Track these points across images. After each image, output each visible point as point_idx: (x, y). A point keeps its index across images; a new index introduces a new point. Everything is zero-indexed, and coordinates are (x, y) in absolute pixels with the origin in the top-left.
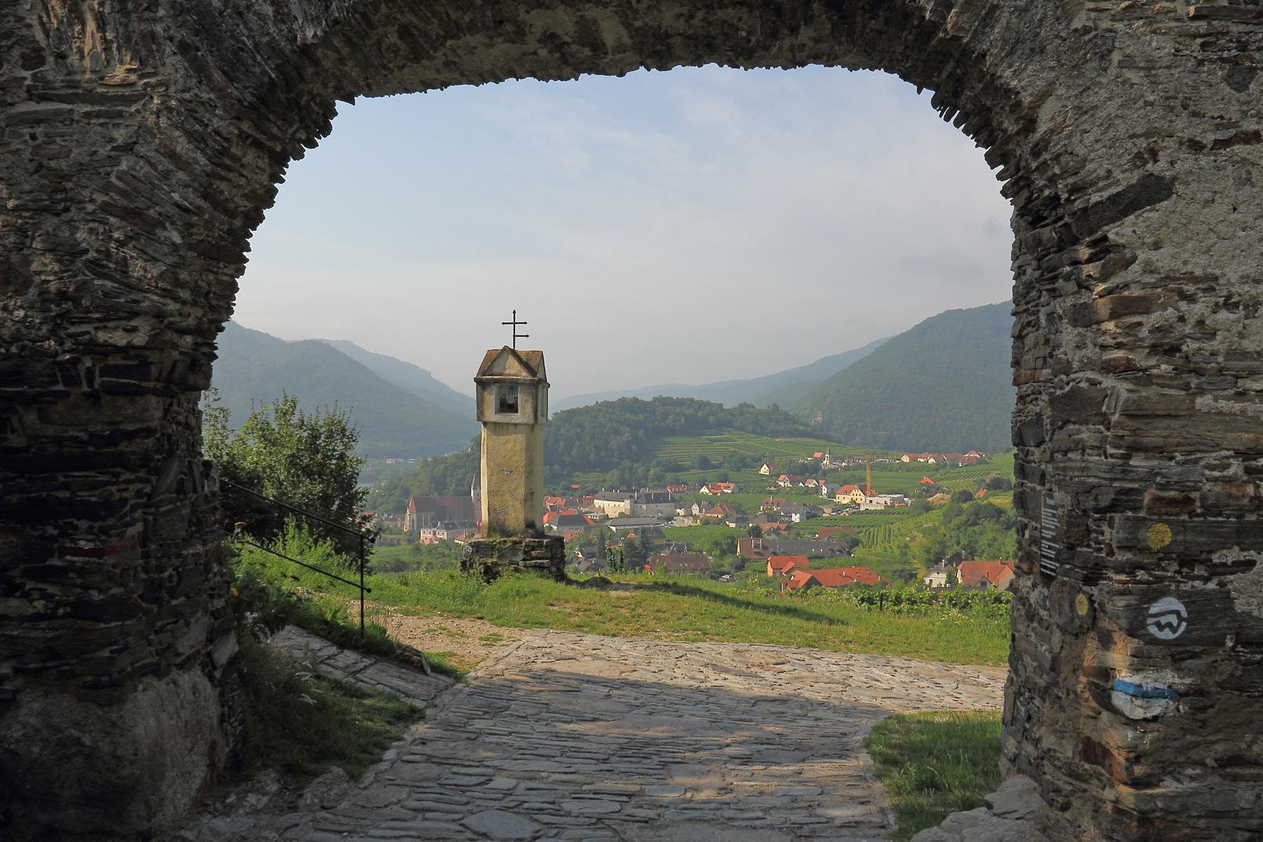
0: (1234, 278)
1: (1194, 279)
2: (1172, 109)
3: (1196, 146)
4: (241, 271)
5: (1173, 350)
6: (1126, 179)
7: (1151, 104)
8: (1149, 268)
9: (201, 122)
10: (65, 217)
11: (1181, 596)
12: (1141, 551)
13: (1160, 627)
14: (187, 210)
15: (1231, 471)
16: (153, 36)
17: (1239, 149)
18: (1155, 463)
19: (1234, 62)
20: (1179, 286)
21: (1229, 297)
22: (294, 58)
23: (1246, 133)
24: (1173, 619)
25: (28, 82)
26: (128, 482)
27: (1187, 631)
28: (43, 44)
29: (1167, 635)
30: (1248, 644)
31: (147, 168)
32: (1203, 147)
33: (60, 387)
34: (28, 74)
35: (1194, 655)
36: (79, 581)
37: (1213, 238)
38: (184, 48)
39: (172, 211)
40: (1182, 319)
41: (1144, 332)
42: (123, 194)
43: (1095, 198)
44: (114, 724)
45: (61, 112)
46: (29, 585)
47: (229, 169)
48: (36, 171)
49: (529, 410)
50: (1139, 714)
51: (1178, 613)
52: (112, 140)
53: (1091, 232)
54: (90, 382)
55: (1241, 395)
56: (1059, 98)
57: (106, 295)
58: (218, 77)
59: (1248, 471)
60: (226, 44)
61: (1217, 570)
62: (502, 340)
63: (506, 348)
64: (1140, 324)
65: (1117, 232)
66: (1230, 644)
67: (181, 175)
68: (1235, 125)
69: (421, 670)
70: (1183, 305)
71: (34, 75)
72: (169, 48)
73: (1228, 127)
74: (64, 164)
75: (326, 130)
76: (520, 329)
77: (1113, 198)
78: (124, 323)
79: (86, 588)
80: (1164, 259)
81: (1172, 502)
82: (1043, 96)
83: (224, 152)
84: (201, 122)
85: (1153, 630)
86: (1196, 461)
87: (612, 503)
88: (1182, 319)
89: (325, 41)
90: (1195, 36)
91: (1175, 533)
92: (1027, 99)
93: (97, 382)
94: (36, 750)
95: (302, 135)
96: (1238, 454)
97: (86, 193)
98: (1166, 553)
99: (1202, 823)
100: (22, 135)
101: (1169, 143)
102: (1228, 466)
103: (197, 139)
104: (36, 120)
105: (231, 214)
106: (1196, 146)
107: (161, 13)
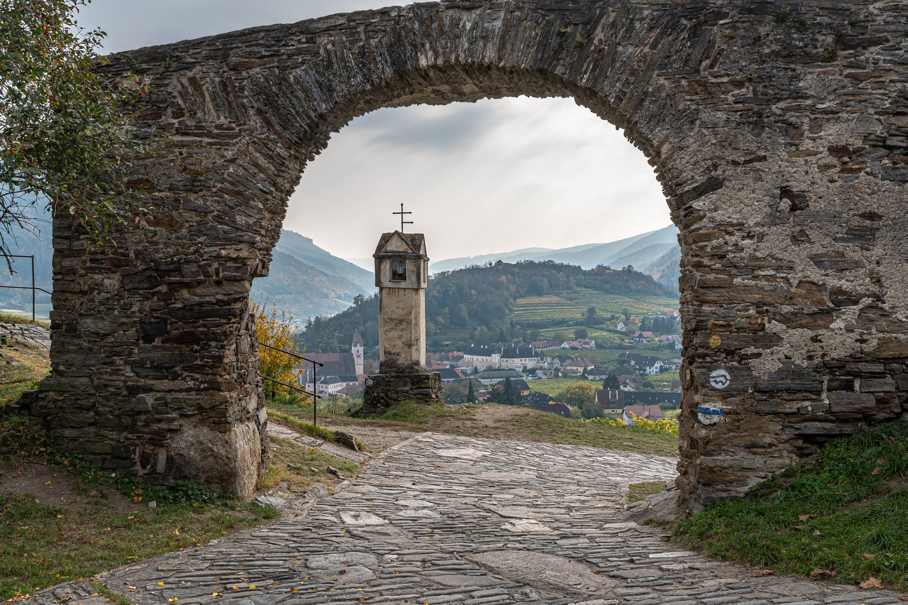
0: (751, 223)
1: (732, 225)
2: (724, 146)
3: (735, 163)
4: (283, 217)
5: (722, 257)
6: (701, 179)
7: (714, 144)
8: (712, 220)
9: (271, 150)
10: (201, 194)
11: (726, 369)
12: (707, 348)
13: (715, 381)
14: (266, 192)
15: (751, 312)
16: (243, 106)
17: (757, 165)
18: (713, 308)
19: (756, 123)
20: (725, 228)
21: (749, 233)
22: (316, 120)
23: (759, 157)
24: (723, 379)
25: (176, 126)
26: (233, 323)
27: (730, 385)
28: (183, 106)
29: (719, 386)
30: (759, 391)
31: (243, 171)
32: (739, 164)
33: (202, 277)
34: (176, 121)
35: (733, 396)
36: (210, 371)
37: (743, 205)
38: (259, 112)
39: (256, 191)
40: (726, 243)
41: (709, 249)
42: (232, 184)
43: (686, 189)
44: (227, 442)
45: (196, 142)
46: (185, 374)
47: (284, 172)
48: (184, 171)
49: (414, 278)
50: (707, 422)
51: (725, 376)
52: (223, 156)
53: (685, 204)
54: (217, 274)
55: (755, 277)
56: (670, 143)
57: (225, 232)
58: (278, 128)
59: (758, 312)
60: (281, 111)
61: (743, 358)
62: (393, 225)
63: (396, 232)
64: (707, 246)
65: (697, 204)
66: (750, 391)
67: (261, 175)
68: (754, 153)
69: (352, 448)
70: (727, 237)
71: (180, 122)
72: (251, 112)
73: (750, 154)
74: (198, 168)
75: (325, 146)
76: (407, 218)
77: (694, 189)
78: (234, 246)
79: (215, 375)
80: (719, 216)
81: (721, 326)
82: (662, 143)
83: (283, 164)
84: (271, 150)
85: (713, 384)
86: (733, 308)
87: (480, 358)
88: (726, 243)
89: (331, 111)
90: (737, 111)
91: (722, 340)
92: (655, 143)
93: (221, 275)
94: (192, 453)
95: (315, 150)
96: (753, 304)
97: (212, 182)
98: (719, 350)
99: (739, 474)
100: (174, 152)
101: (723, 162)
102: (748, 310)
103: (269, 157)
104: (182, 145)
105: (282, 191)
106: (735, 163)
107: (246, 93)
